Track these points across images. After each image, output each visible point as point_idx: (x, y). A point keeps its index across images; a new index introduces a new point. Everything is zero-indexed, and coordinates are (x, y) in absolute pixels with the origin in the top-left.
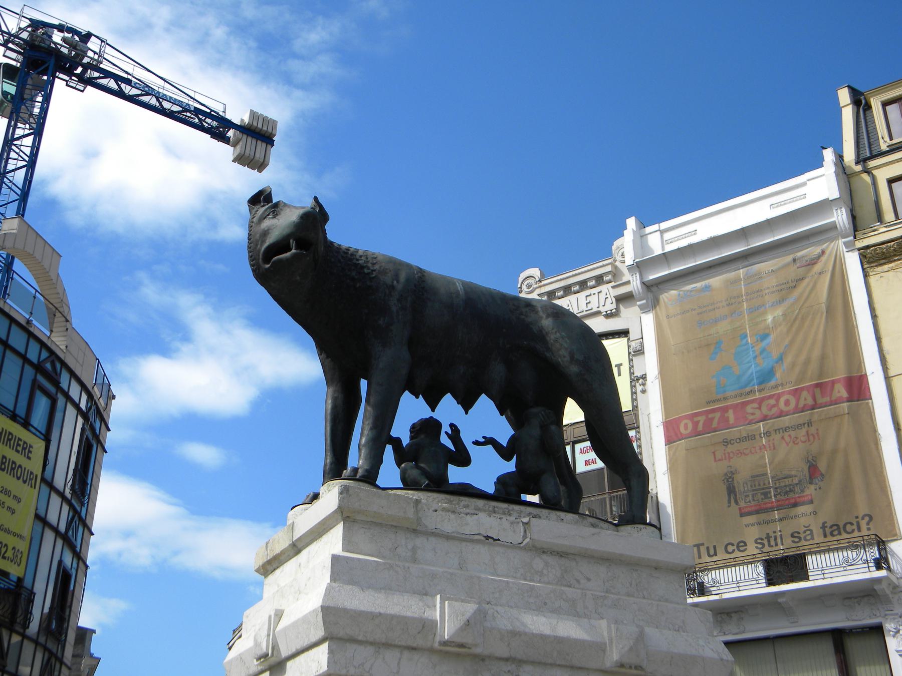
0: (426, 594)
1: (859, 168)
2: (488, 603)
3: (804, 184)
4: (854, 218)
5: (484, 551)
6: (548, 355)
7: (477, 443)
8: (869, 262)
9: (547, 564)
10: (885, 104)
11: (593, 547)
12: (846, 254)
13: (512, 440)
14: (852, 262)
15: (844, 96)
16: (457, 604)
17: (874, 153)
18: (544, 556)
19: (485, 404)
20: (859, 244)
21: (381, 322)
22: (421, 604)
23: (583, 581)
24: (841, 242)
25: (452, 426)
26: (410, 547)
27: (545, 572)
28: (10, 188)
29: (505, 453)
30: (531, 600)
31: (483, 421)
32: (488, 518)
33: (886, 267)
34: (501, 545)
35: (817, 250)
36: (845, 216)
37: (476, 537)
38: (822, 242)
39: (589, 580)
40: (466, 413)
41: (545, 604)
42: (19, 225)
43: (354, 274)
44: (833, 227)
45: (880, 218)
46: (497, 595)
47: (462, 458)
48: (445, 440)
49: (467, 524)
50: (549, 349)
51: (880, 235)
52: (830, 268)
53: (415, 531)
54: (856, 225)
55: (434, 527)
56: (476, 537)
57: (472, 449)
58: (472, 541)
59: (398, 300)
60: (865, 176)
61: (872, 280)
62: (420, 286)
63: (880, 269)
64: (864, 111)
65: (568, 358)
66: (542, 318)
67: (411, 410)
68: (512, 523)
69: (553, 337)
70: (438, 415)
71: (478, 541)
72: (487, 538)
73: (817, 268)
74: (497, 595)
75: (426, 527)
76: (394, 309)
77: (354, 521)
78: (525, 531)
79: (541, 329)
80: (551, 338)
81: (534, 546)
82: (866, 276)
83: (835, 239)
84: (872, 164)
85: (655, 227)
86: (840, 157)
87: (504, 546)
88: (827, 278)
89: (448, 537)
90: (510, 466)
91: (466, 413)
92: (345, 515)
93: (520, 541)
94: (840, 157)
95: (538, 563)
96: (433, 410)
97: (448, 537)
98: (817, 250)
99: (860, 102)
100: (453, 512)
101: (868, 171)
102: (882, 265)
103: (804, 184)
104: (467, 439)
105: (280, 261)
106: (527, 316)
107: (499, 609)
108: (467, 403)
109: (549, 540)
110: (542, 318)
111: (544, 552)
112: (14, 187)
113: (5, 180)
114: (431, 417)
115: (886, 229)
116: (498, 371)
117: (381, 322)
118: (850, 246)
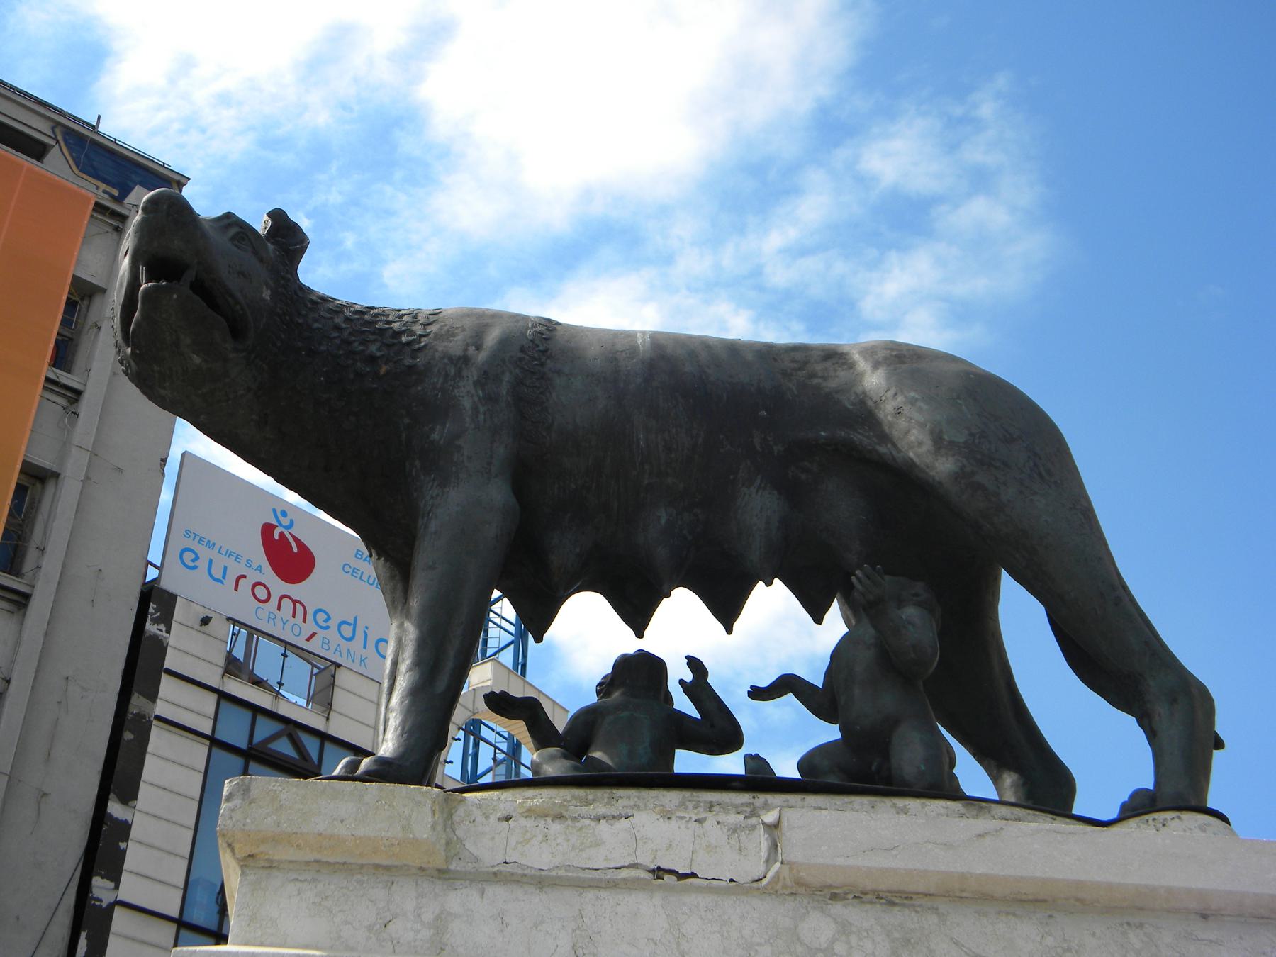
5: (650, 910)
6: (882, 449)
9: (844, 928)
11: (980, 869)
18: (837, 908)
19: (771, 602)
21: (435, 436)
26: (428, 916)
28: (499, 626)
32: (663, 825)
34: (700, 890)
37: (624, 874)
40: (729, 630)
42: (494, 673)
43: (373, 348)
48: (683, 703)
49: (598, 844)
50: (885, 438)
53: (443, 874)
55: (500, 859)
56: (624, 874)
57: (746, 713)
58: (612, 885)
59: (477, 384)
62: (537, 353)
65: (928, 445)
66: (862, 375)
68: (734, 830)
69: (889, 407)
72: (659, 872)
75: (477, 860)
76: (467, 403)
77: (271, 866)
80: (886, 412)
81: (799, 883)
87: (709, 890)
89: (542, 881)
90: (830, 733)
91: (729, 630)
96: (640, 635)
97: (542, 881)
100: (559, 817)
105: (138, 324)
106: (825, 378)
108: (726, 609)
109: (840, 861)
111: (834, 897)
112: (504, 624)
113: (492, 615)
116: (759, 507)
117: (435, 436)
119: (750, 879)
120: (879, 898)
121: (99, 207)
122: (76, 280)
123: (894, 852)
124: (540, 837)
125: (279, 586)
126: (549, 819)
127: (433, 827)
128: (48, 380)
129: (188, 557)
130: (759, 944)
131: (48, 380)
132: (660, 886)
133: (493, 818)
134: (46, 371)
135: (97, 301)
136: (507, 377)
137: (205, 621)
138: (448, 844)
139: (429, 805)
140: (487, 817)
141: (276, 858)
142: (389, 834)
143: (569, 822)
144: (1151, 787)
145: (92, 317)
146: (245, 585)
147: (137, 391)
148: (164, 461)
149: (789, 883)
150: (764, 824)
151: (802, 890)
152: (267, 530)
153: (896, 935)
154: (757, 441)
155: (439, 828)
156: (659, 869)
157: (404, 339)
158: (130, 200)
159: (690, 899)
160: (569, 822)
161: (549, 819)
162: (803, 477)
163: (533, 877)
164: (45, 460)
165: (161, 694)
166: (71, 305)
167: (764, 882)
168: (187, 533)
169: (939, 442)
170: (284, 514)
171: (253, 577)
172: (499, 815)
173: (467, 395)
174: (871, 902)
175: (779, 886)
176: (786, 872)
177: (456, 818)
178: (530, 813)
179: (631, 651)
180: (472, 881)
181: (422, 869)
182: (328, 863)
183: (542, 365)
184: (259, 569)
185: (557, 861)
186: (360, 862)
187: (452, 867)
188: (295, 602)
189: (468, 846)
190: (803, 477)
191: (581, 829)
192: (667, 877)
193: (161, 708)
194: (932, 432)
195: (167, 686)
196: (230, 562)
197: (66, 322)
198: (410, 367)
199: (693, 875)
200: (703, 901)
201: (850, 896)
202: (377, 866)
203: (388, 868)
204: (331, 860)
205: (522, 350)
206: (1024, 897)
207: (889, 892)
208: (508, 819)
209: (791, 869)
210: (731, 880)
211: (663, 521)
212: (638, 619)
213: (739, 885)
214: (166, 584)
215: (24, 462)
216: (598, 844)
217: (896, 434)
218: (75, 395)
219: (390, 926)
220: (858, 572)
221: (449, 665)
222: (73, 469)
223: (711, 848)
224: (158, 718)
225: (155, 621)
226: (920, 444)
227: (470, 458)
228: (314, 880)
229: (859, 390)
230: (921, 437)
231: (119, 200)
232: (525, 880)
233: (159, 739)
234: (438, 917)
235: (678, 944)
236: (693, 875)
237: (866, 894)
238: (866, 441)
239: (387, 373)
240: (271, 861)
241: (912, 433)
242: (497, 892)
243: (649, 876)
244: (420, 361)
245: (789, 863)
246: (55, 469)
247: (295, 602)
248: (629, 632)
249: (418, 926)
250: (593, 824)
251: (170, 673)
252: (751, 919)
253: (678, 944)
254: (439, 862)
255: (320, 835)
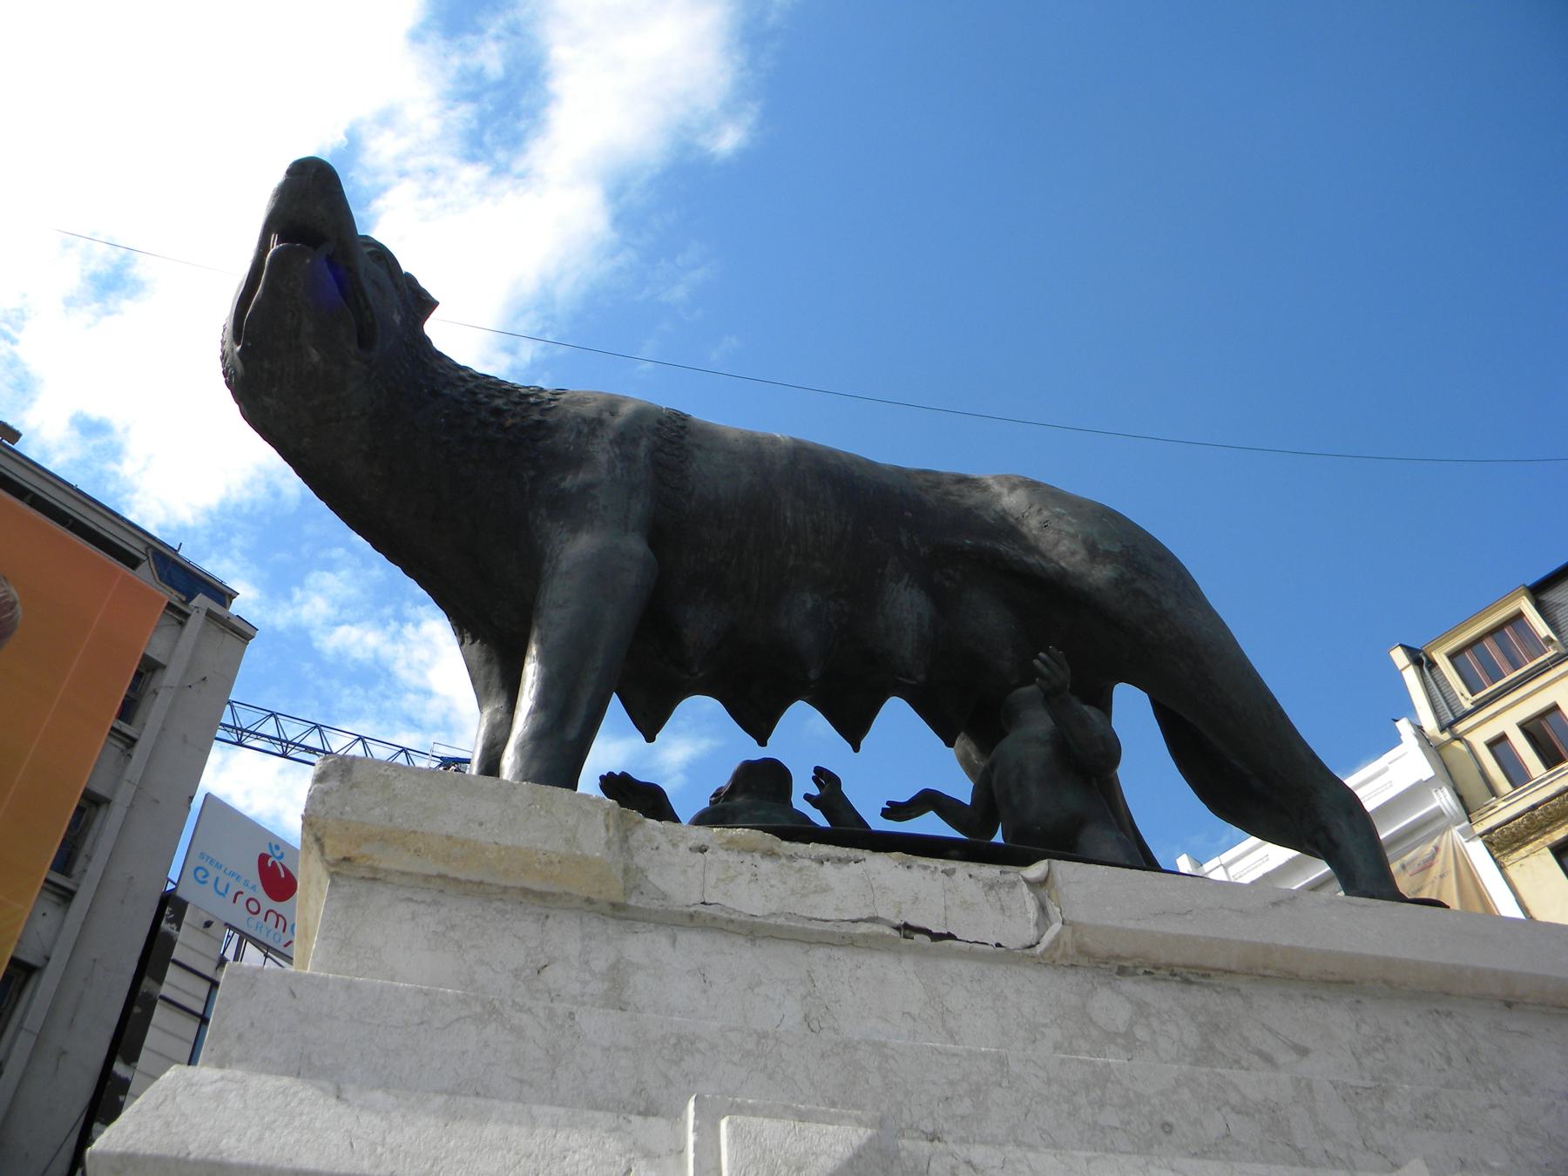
0: (648, 1112)
1: (1446, 736)
2: (933, 1137)
3: (1385, 770)
4: (1461, 798)
5: (901, 977)
6: (1031, 560)
8: (1499, 850)
9: (1141, 1009)
10: (1452, 657)
11: (1285, 941)
12: (1468, 846)
14: (1478, 853)
15: (1399, 657)
16: (771, 1130)
17: (1459, 714)
18: (1127, 985)
19: (897, 719)
20: (1479, 829)
22: (612, 1145)
23: (1284, 1057)
24: (1455, 831)
26: (600, 965)
27: (1141, 1033)
30: (1109, 1117)
33: (1523, 852)
34: (960, 955)
35: (1429, 848)
36: (1449, 797)
37: (863, 928)
38: (1430, 837)
39: (1303, 1052)
40: (856, 748)
41: (1167, 1128)
44: (1439, 814)
45: (1493, 791)
46: (964, 1107)
49: (825, 890)
50: (1032, 549)
51: (1503, 812)
52: (1452, 867)
53: (620, 912)
54: (1468, 808)
55: (696, 897)
56: (863, 928)
58: (849, 942)
60: (1457, 744)
61: (1511, 871)
63: (1515, 855)
64: (1430, 669)
65: (1082, 554)
66: (999, 495)
68: (991, 886)
70: (776, 748)
71: (870, 944)
72: (907, 930)
73: (1436, 870)
74: (964, 1107)
75: (665, 897)
76: (603, 458)
77: (375, 877)
78: (1043, 908)
79: (1003, 517)
80: (1032, 524)
81: (1082, 950)
82: (1501, 868)
83: (1442, 831)
84: (1460, 727)
85: (1215, 862)
86: (1419, 729)
87: (971, 955)
88: (1452, 879)
89: (754, 931)
91: (856, 748)
92: (335, 850)
94: (1419, 729)
95: (1111, 1005)
96: (763, 743)
97: (754, 931)
98: (1429, 848)
99: (1420, 660)
101: (1458, 738)
102: (1516, 849)
103: (1385, 770)
107: (978, 1153)
108: (853, 728)
109: (1131, 924)
110: (999, 495)
111: (1122, 971)
118: (1469, 835)
119: (1019, 944)
120: (1173, 974)
121: (170, 606)
122: (145, 657)
123: (1189, 917)
124: (748, 876)
125: (267, 903)
126: (757, 855)
127: (608, 843)
128: (113, 729)
129: (201, 873)
130: (1045, 1025)
131: (113, 729)
133: (683, 848)
134: (113, 721)
135: (158, 674)
136: (644, 442)
137: (208, 924)
138: (626, 871)
139: (601, 817)
140: (675, 845)
141: (383, 865)
142: (547, 847)
143: (784, 861)
145: (153, 686)
146: (242, 899)
148: (191, 798)
149: (1070, 950)
150: (1026, 881)
151: (1084, 961)
152: (263, 858)
153: (1201, 1019)
154: (904, 539)
155: (615, 848)
156: (906, 926)
157: (532, 400)
158: (194, 603)
159: (952, 966)
160: (784, 861)
161: (757, 855)
162: (947, 584)
163: (742, 924)
164: (100, 789)
165: (167, 978)
166: (138, 675)
167: (1039, 949)
168: (202, 855)
169: (1093, 551)
170: (277, 847)
171: (248, 894)
172: (690, 844)
173: (602, 451)
174: (1165, 980)
175: (1058, 954)
176: (1067, 937)
177: (633, 842)
178: (730, 845)
180: (659, 924)
181: (589, 901)
182: (456, 880)
183: (681, 437)
184: (254, 888)
185: (773, 907)
186: (504, 882)
187: (632, 902)
188: (278, 916)
189: (651, 877)
190: (947, 584)
191: (800, 869)
192: (917, 937)
193: (165, 990)
194: (1085, 541)
195: (172, 972)
196: (232, 880)
197: (133, 687)
198: (539, 422)
199: (950, 936)
200: (967, 968)
201: (1141, 971)
202: (526, 891)
203: (542, 896)
204: (462, 876)
205: (659, 422)
206: (1331, 978)
207: (1185, 966)
208: (703, 850)
209: (1074, 932)
210: (998, 945)
211: (809, 606)
212: (760, 729)
213: (1008, 950)
214: (181, 893)
215: (86, 790)
216: (825, 890)
217: (1043, 546)
218: (131, 742)
219: (547, 973)
220: (1041, 654)
221: (582, 711)
222: (122, 798)
223: (967, 906)
224: (163, 998)
225: (169, 921)
226: (1074, 553)
227: (605, 508)
228: (435, 903)
229: (999, 508)
230: (1074, 547)
231: (186, 603)
232: (731, 927)
233: (160, 1014)
234: (614, 967)
235: (944, 1022)
237: (1158, 968)
238: (1012, 552)
239: (514, 425)
240: (375, 870)
241: (1063, 549)
242: (695, 942)
244: (551, 419)
245: (1072, 924)
246: (108, 796)
247: (278, 916)
249: (587, 977)
250: (815, 865)
251: (176, 962)
252: (1032, 993)
253: (944, 1022)
254: (616, 895)
255: (449, 837)
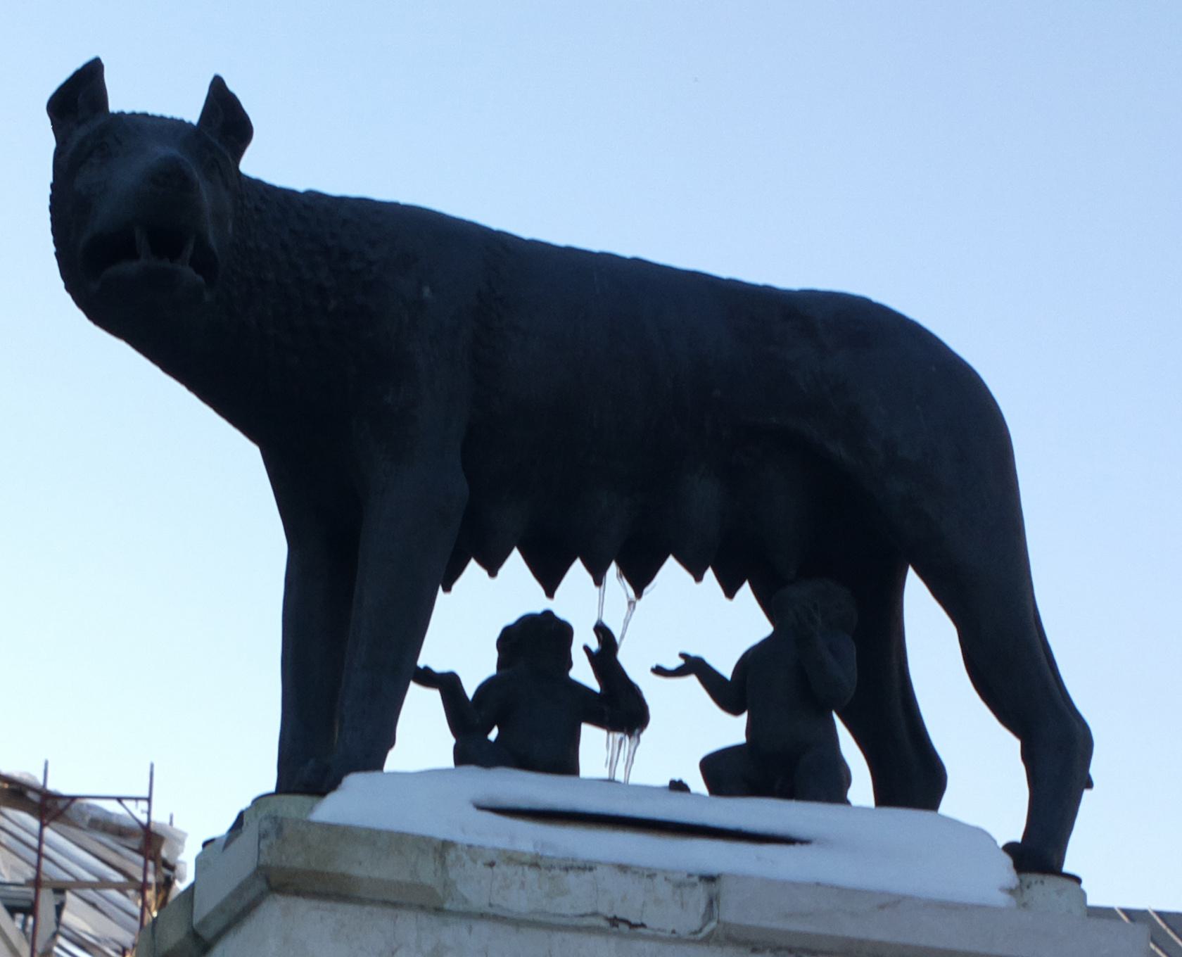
7: (659, 671)
13: (751, 661)
25: (602, 631)
29: (727, 693)
31: (683, 625)
37: (586, 922)
47: (623, 710)
57: (653, 690)
58: (578, 929)
67: (467, 625)
71: (591, 930)
72: (614, 921)
75: (466, 901)
87: (654, 938)
89: (518, 922)
93: (696, 927)
96: (550, 593)
97: (518, 922)
104: (635, 663)
114: (548, 614)
115: (114, 846)
132: (615, 934)
133: (479, 863)
140: (475, 861)
144: (115, 106)
147: (50, 127)
156: (615, 918)
159: (641, 945)
179: (538, 609)
199: (643, 925)
208: (492, 865)
236: (643, 925)
242: (483, 928)
243: (604, 924)
248: (539, 590)
250: (563, 873)
